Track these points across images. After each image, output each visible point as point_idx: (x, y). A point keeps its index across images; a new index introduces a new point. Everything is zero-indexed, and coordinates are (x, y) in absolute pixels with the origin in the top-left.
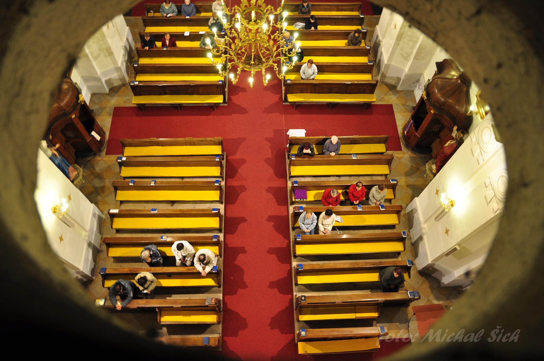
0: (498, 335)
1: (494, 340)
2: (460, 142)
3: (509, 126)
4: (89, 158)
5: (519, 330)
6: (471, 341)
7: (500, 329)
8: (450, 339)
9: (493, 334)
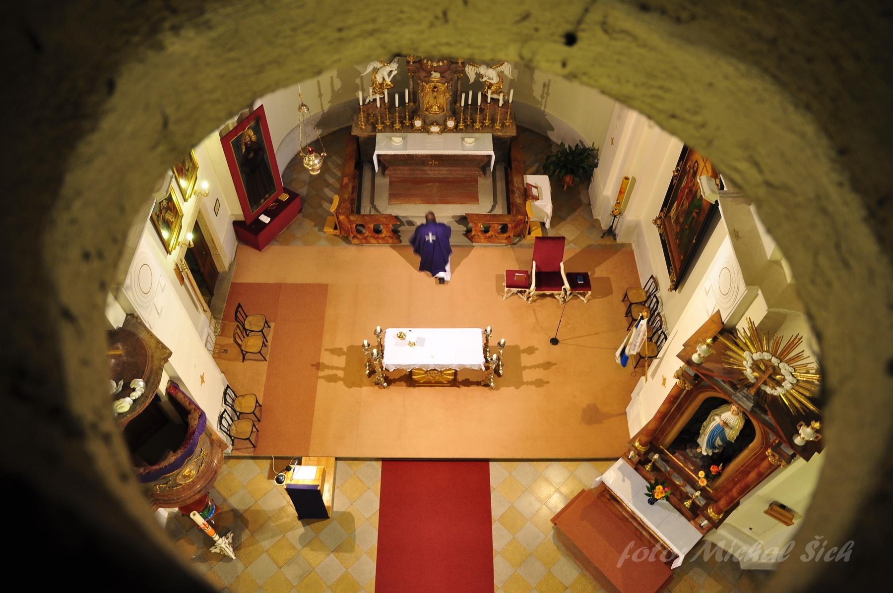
4: (812, 552)
5: (853, 543)
7: (821, 541)
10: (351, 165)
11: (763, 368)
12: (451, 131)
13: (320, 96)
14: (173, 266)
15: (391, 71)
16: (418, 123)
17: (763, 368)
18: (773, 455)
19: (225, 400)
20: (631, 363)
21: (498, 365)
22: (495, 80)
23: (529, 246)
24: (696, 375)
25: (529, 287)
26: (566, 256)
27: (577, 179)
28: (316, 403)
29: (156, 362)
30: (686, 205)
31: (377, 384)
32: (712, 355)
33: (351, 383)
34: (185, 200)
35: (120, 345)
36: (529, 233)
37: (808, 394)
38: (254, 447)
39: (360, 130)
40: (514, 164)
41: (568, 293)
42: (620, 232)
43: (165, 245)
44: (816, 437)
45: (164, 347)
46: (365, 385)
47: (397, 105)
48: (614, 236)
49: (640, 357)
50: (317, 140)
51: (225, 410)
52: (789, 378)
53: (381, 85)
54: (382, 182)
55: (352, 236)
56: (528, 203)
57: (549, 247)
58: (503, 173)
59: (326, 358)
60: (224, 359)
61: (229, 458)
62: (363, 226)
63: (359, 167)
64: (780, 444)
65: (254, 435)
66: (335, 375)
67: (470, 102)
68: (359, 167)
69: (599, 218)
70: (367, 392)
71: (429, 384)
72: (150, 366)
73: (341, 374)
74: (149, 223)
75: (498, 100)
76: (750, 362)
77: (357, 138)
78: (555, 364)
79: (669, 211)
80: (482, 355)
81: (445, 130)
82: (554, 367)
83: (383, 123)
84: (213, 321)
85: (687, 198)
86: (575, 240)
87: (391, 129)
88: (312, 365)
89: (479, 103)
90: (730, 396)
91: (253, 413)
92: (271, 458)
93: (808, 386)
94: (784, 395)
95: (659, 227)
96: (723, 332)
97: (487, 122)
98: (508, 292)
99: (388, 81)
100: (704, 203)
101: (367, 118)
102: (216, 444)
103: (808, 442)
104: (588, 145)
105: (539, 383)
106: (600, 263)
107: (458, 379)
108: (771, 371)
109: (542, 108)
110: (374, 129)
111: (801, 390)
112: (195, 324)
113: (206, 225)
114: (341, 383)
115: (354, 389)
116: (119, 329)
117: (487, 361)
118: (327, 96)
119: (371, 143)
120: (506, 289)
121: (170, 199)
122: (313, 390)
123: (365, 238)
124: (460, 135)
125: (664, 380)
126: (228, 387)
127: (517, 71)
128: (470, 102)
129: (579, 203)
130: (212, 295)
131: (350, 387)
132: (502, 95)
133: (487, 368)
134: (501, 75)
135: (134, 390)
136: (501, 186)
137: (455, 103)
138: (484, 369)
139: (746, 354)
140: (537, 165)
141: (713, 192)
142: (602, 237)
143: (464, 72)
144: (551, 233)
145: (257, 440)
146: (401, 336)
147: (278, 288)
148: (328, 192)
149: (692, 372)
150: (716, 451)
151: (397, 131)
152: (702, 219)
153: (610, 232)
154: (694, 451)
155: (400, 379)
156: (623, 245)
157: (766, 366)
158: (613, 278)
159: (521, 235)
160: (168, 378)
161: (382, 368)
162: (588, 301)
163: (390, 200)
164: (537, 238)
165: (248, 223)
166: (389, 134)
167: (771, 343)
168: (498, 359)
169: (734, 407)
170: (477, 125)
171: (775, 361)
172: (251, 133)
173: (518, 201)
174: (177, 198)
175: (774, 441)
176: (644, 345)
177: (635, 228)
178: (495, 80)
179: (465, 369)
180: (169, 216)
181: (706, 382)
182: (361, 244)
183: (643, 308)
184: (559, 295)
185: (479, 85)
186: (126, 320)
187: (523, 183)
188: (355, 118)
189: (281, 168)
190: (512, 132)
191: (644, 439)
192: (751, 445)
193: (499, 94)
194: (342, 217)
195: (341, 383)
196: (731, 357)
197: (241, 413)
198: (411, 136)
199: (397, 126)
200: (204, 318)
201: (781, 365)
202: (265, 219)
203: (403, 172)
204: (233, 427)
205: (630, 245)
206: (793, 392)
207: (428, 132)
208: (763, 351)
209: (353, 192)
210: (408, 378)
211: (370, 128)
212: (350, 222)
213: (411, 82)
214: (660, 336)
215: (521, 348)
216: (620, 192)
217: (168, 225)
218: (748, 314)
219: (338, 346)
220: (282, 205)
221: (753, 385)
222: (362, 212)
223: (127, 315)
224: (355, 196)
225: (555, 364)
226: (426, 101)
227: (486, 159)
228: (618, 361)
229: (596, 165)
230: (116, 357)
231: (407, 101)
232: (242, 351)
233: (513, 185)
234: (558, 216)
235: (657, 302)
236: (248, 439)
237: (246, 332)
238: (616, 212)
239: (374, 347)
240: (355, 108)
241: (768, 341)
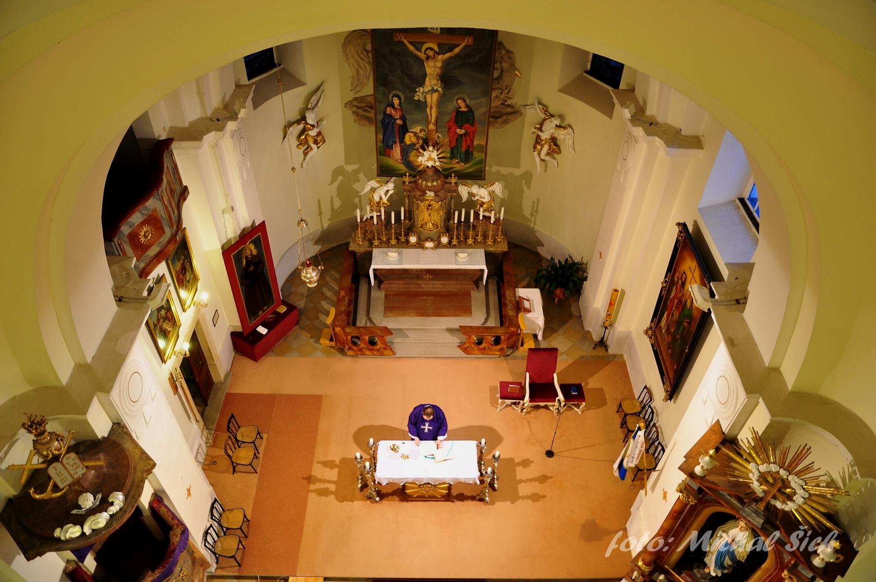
0: (801, 540)
1: (795, 548)
2: (666, 277)
3: (120, 300)
6: (758, 550)
7: (805, 531)
8: (725, 546)
10: (348, 279)
11: (771, 481)
12: (445, 246)
13: (320, 214)
14: (168, 375)
15: (388, 191)
16: (413, 239)
17: (771, 481)
18: (791, 578)
19: (212, 514)
20: (629, 476)
21: (493, 479)
22: (487, 199)
23: (522, 358)
24: (700, 488)
25: (523, 399)
26: (560, 366)
27: (567, 292)
28: (306, 518)
29: (139, 474)
30: (676, 315)
31: (369, 498)
32: (715, 467)
33: (343, 497)
34: (184, 310)
35: (102, 456)
36: (522, 345)
37: (822, 510)
38: (240, 565)
39: (358, 245)
40: (506, 278)
41: (563, 404)
42: (611, 342)
43: (161, 354)
44: (837, 559)
45: (149, 458)
46: (357, 500)
47: (393, 222)
48: (606, 347)
49: (638, 470)
50: (316, 256)
51: (211, 526)
52: (800, 492)
53: (378, 203)
54: (378, 295)
55: (347, 347)
56: (520, 315)
57: (542, 358)
58: (496, 287)
59: (318, 471)
60: (213, 471)
61: (211, 577)
62: (357, 337)
63: (356, 281)
64: (796, 565)
65: (240, 553)
66: (327, 489)
67: (463, 220)
68: (356, 281)
69: (591, 330)
70: (359, 506)
71: (422, 498)
72: (132, 477)
73: (332, 487)
74: (143, 332)
75: (490, 218)
76: (757, 474)
77: (354, 253)
78: (551, 477)
79: (659, 321)
80: (477, 469)
81: (439, 245)
82: (550, 481)
83: (379, 239)
84: (206, 431)
85: (677, 308)
86: (568, 352)
87: (387, 244)
88: (304, 478)
89: (472, 220)
90: (738, 512)
91: (240, 528)
92: (256, 578)
93: (821, 501)
94: (796, 510)
95: (651, 338)
96: (725, 442)
97: (480, 239)
98: (502, 404)
99: (385, 200)
100: (695, 312)
101: (365, 234)
102: (198, 563)
103: (828, 564)
104: (577, 259)
105: (535, 498)
106: (593, 374)
107: (453, 494)
108: (780, 484)
109: (532, 225)
110: (371, 244)
111: (814, 505)
112: (186, 435)
113: (204, 336)
114: (332, 497)
115: (346, 503)
116: (104, 438)
117: (482, 475)
118: (327, 215)
119: (368, 258)
120: (500, 401)
121: (169, 309)
122: (304, 503)
123: (360, 350)
124: (453, 250)
125: (665, 494)
126: (216, 500)
127: (507, 192)
128: (463, 220)
129: (571, 316)
130: (206, 405)
131: (341, 501)
132: (493, 213)
133: (482, 482)
134: (492, 194)
135: (112, 504)
136: (493, 299)
137: (449, 220)
138: (478, 482)
139: (751, 466)
140: (528, 279)
141: (705, 300)
142: (594, 349)
143: (456, 191)
144: (544, 345)
145: (242, 559)
146: (394, 449)
147: (271, 400)
148: (325, 304)
149: (695, 486)
150: (726, 571)
151: (393, 246)
152: (693, 328)
153: (602, 343)
154: (701, 571)
155: (393, 494)
156: (615, 356)
157: (774, 479)
158: (606, 389)
159: (514, 347)
160: (152, 491)
161: (374, 481)
162: (583, 412)
163: (385, 312)
164: (530, 349)
165: (245, 335)
166: (385, 250)
167: (778, 453)
168: (493, 472)
169: (742, 524)
170: (470, 241)
171: (783, 473)
172: (252, 247)
173: (511, 313)
174: (176, 308)
175: (789, 562)
176: (642, 458)
177: (627, 338)
178: (487, 199)
179: (459, 483)
180: (166, 326)
181: (711, 496)
182: (356, 356)
183: (636, 418)
184: (554, 406)
185: (471, 204)
186: (112, 429)
187: (515, 297)
188: (353, 234)
189: (280, 282)
190: (503, 247)
191: (648, 558)
192: (764, 566)
193: (490, 212)
194: (338, 329)
195: (332, 497)
196: (736, 469)
197: (228, 529)
198: (407, 252)
199: (393, 242)
200: (196, 428)
201: (790, 478)
202: (262, 330)
203: (398, 286)
204: (219, 544)
205: (622, 356)
206: (806, 507)
207: (423, 247)
208: (770, 463)
209: (349, 305)
210: (401, 493)
211: (367, 243)
212: (346, 334)
213: (407, 201)
214: (657, 448)
215: (516, 461)
216: (611, 304)
217: (165, 334)
218: (750, 424)
219: (330, 458)
220: (280, 317)
221: (761, 499)
222: (358, 324)
223: (114, 424)
224: (352, 308)
225: (551, 477)
226: (420, 219)
227: (479, 273)
228: (616, 474)
229: (585, 279)
230: (97, 468)
231: (402, 218)
232: (233, 462)
233: (505, 298)
234: (550, 328)
235: (652, 412)
236: (233, 557)
237: (238, 443)
238: (607, 324)
239: (366, 460)
240: (353, 225)
241: (774, 451)
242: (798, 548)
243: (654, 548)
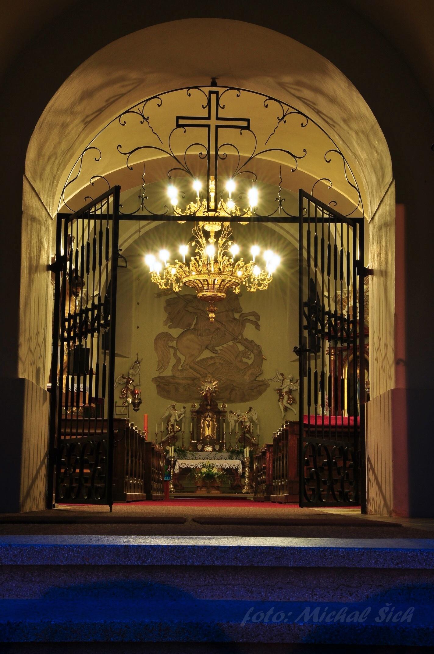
0: (387, 614)
5: (413, 608)
6: (355, 621)
7: (390, 607)
9: (381, 612)
110: (264, 453)
145: (106, 196)
224: (134, 499)
242: (385, 619)
243: (355, 614)
